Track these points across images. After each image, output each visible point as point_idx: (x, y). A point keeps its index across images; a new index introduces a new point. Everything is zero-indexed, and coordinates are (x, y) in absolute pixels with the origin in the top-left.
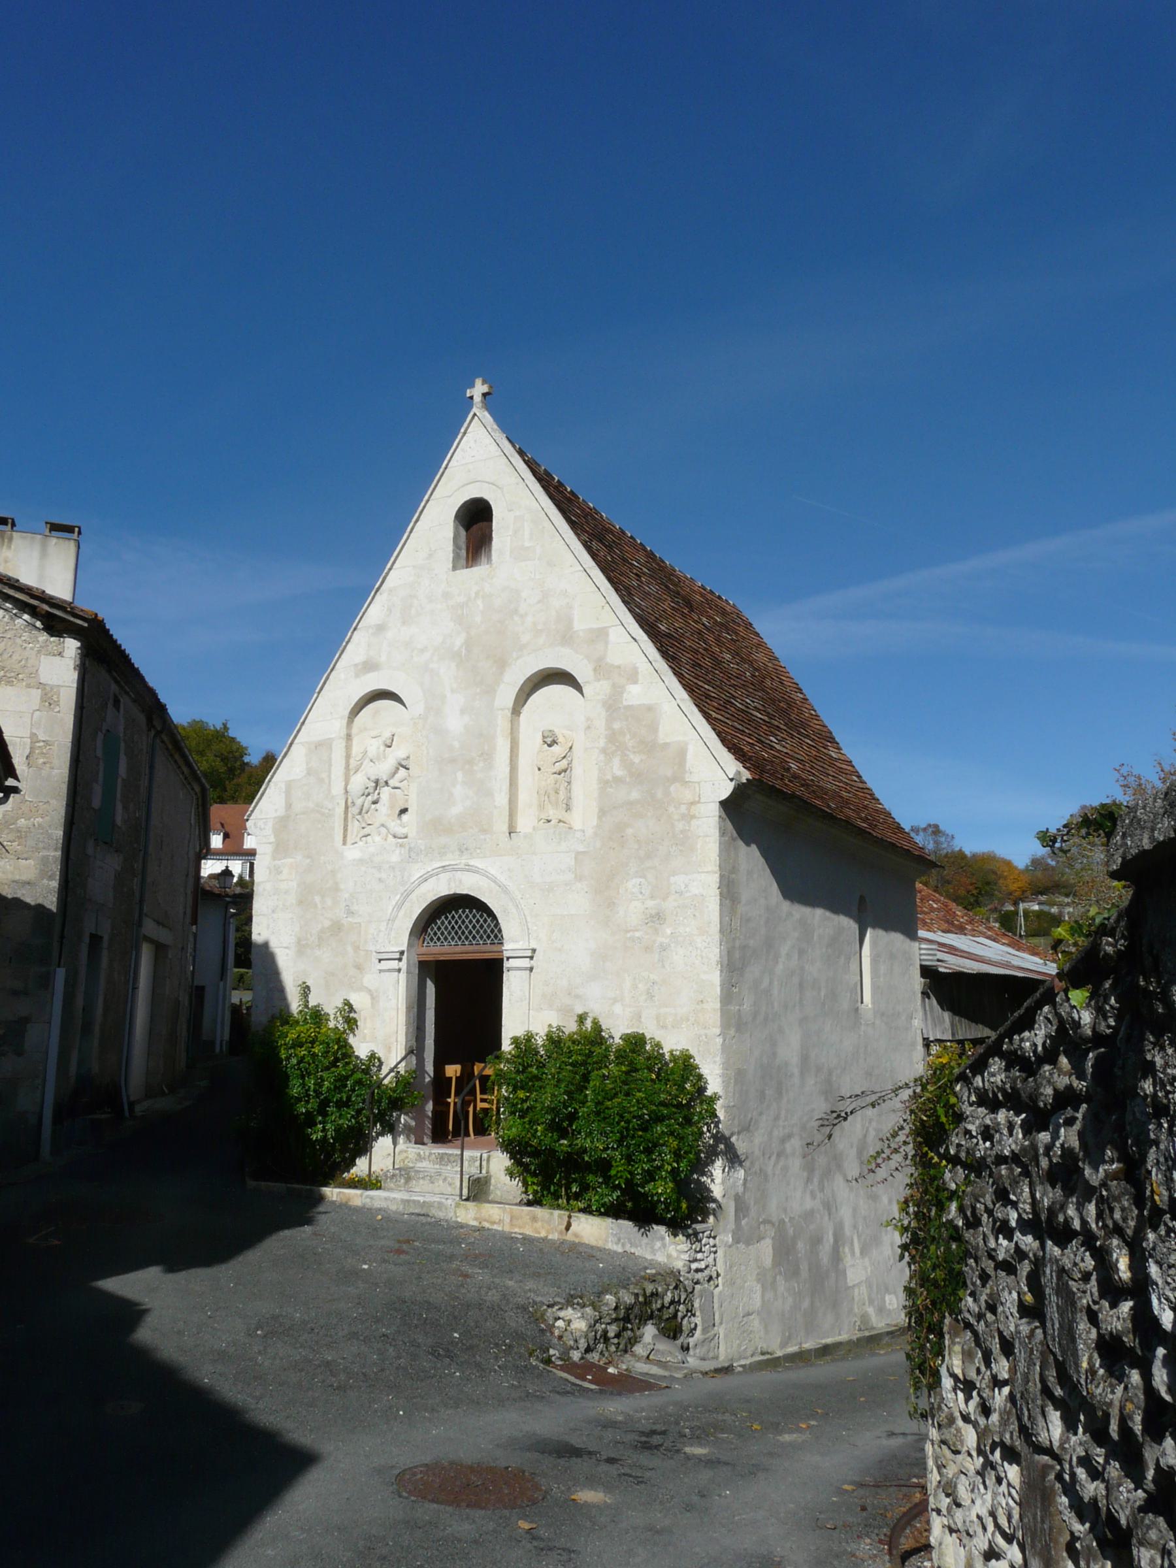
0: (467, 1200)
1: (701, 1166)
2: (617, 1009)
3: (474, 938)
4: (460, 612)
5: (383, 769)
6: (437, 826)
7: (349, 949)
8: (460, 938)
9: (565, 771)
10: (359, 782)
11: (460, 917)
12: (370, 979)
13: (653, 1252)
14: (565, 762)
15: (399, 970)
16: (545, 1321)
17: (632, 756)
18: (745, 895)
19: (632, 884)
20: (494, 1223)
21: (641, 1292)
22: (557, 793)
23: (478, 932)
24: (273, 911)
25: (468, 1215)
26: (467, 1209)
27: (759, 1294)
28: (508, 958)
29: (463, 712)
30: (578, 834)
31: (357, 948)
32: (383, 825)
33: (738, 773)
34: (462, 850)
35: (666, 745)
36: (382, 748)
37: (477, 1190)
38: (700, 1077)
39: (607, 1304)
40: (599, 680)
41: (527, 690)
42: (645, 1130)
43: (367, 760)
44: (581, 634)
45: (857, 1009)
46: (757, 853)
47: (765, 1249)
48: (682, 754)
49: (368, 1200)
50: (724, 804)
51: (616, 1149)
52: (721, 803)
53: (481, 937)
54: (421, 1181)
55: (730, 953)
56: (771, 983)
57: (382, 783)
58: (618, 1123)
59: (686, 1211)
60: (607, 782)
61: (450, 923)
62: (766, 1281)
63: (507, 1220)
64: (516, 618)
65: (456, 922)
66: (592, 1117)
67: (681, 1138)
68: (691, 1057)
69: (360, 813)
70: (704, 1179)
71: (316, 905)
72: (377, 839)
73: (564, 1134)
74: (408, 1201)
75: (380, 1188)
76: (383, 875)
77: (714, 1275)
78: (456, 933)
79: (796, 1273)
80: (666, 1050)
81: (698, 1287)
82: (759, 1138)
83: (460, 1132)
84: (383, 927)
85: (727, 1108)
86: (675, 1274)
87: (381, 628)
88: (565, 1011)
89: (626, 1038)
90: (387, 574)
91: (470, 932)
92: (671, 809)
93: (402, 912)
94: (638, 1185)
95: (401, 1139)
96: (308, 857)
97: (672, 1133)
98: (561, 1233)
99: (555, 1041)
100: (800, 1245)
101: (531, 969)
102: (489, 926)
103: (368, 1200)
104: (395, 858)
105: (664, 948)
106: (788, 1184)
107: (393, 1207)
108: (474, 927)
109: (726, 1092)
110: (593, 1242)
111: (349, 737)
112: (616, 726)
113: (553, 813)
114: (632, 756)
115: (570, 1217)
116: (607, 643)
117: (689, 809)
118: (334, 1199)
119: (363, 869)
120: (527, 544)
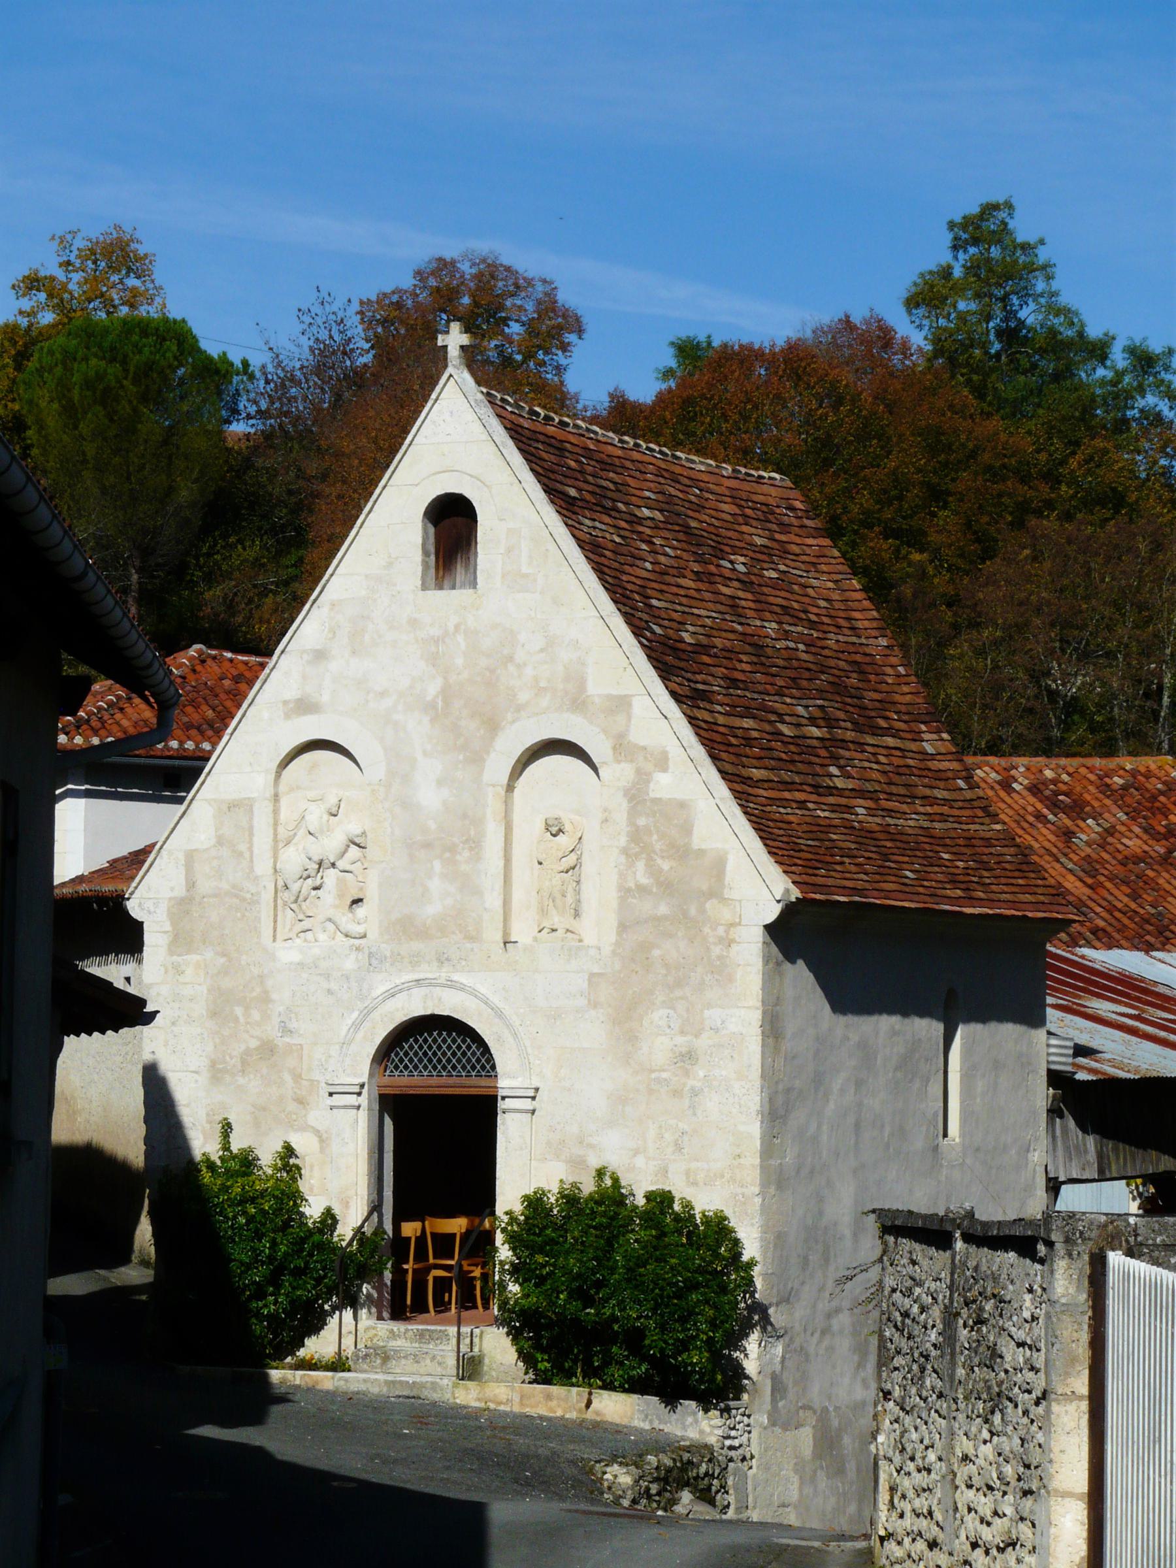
0: (462, 1379)
1: (736, 1339)
2: (640, 1161)
3: (454, 1068)
4: (433, 649)
5: (330, 846)
6: (406, 928)
7: (287, 1078)
8: (435, 1068)
9: (573, 868)
10: (293, 859)
11: (435, 1041)
12: (318, 1115)
13: (684, 1428)
14: (573, 857)
15: (358, 1107)
16: (594, 1474)
17: (659, 861)
18: (790, 1027)
19: (659, 1016)
20: (500, 1403)
21: (678, 1458)
22: (564, 896)
23: (459, 1061)
24: (173, 1024)
25: (468, 1396)
26: (467, 1389)
27: (796, 1485)
28: (503, 1098)
29: (440, 783)
30: (592, 952)
31: (297, 1077)
32: (330, 920)
33: (787, 891)
34: (442, 960)
35: (701, 853)
36: (326, 817)
37: (470, 1368)
38: (737, 1242)
39: (649, 1463)
40: (619, 762)
41: (524, 760)
42: (679, 1298)
43: (302, 832)
44: (597, 700)
45: (936, 1148)
46: (809, 977)
47: (805, 1438)
48: (719, 867)
49: (342, 1383)
50: (769, 928)
51: (650, 1318)
52: (767, 927)
53: (464, 1068)
54: (403, 1361)
55: (771, 1100)
56: (819, 1127)
57: (326, 864)
58: (653, 1290)
59: (721, 1387)
60: (629, 890)
61: (421, 1047)
62: (807, 1479)
63: (516, 1399)
64: (511, 668)
65: (430, 1048)
66: (624, 1285)
67: (715, 1307)
68: (726, 1218)
69: (296, 901)
70: (737, 1354)
71: (237, 1020)
72: (322, 937)
73: (589, 1301)
74: (393, 1382)
75: (349, 1370)
76: (334, 986)
77: (748, 1456)
78: (430, 1061)
79: (840, 1471)
80: (697, 1212)
81: (731, 1465)
82: (800, 1312)
83: (420, 1307)
84: (334, 1050)
85: (765, 1275)
86: (708, 1448)
87: (320, 655)
88: (578, 1163)
89: (649, 1197)
90: (328, 581)
91: (449, 1061)
92: (707, 930)
93: (360, 1035)
94: (670, 1357)
95: (363, 1313)
96: (224, 955)
97: (707, 1302)
98: (580, 1411)
99: (570, 1199)
100: (846, 1440)
101: (533, 1112)
102: (474, 1054)
103: (342, 1383)
104: (350, 964)
105: (695, 1093)
106: (834, 1367)
107: (375, 1390)
108: (454, 1054)
109: (765, 1258)
110: (617, 1420)
111: (276, 797)
112: (642, 822)
113: (556, 920)
114: (659, 861)
115: (590, 1394)
116: (629, 718)
117: (727, 932)
118: (298, 1382)
119: (305, 975)
120: (525, 570)
